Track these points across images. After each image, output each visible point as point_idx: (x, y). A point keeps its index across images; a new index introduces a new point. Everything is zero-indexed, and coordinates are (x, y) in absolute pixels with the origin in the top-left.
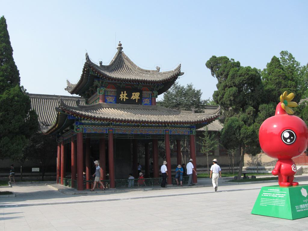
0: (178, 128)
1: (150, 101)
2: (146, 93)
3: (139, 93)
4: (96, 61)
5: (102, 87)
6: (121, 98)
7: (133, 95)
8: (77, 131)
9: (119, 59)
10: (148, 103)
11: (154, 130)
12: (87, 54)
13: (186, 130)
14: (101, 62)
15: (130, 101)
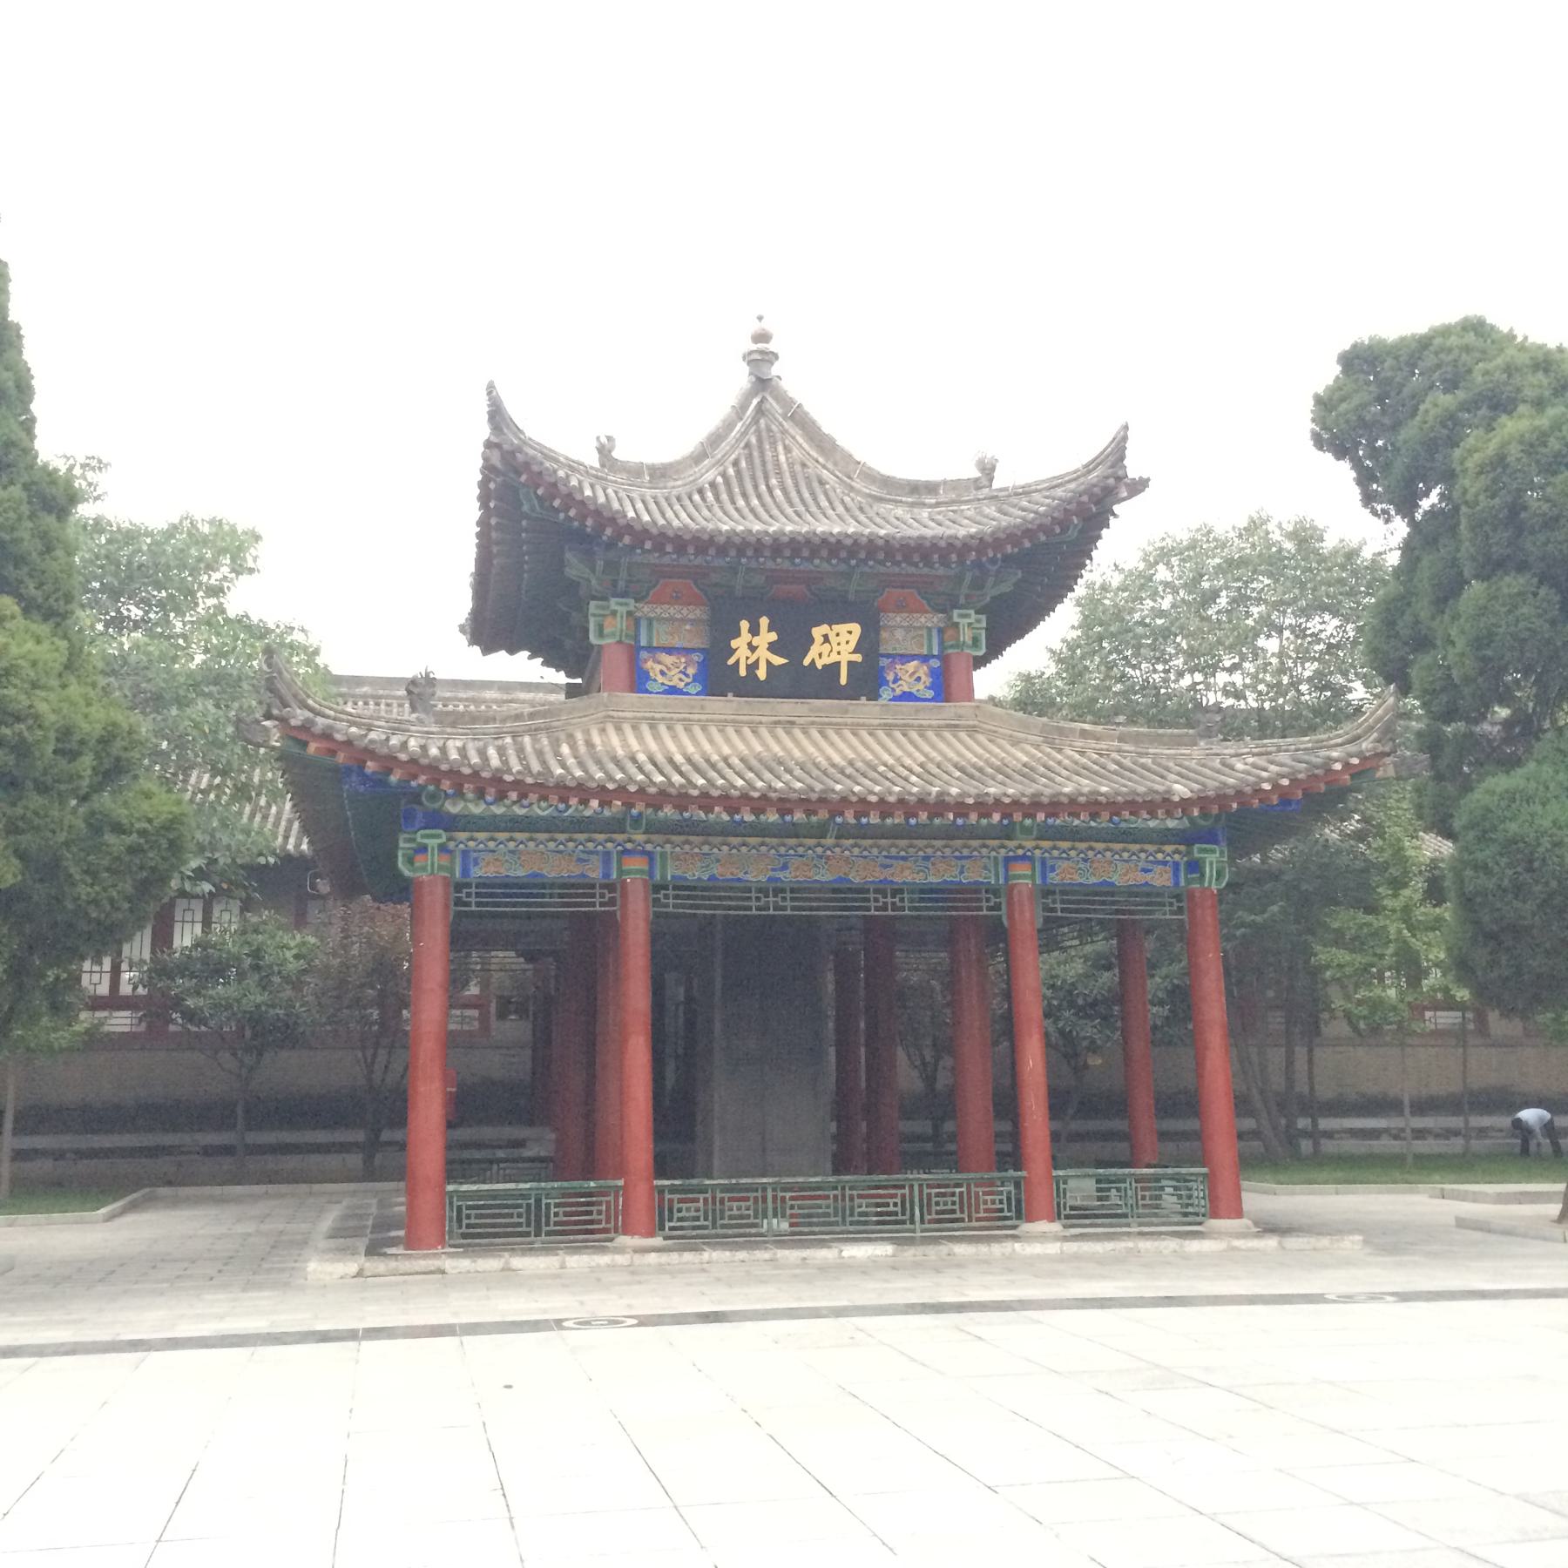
0: (1100, 846)
1: (933, 673)
2: (901, 632)
3: (856, 628)
4: (563, 434)
5: (615, 595)
6: (738, 662)
7: (818, 638)
8: (414, 871)
9: (755, 421)
10: (921, 686)
11: (927, 858)
12: (491, 389)
13: (1160, 856)
14: (609, 438)
15: (800, 682)
